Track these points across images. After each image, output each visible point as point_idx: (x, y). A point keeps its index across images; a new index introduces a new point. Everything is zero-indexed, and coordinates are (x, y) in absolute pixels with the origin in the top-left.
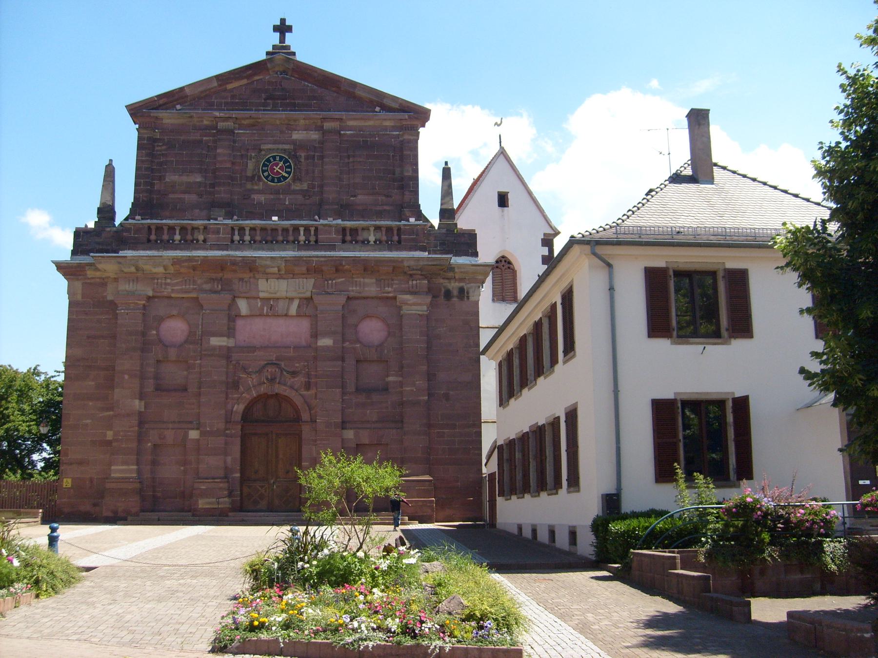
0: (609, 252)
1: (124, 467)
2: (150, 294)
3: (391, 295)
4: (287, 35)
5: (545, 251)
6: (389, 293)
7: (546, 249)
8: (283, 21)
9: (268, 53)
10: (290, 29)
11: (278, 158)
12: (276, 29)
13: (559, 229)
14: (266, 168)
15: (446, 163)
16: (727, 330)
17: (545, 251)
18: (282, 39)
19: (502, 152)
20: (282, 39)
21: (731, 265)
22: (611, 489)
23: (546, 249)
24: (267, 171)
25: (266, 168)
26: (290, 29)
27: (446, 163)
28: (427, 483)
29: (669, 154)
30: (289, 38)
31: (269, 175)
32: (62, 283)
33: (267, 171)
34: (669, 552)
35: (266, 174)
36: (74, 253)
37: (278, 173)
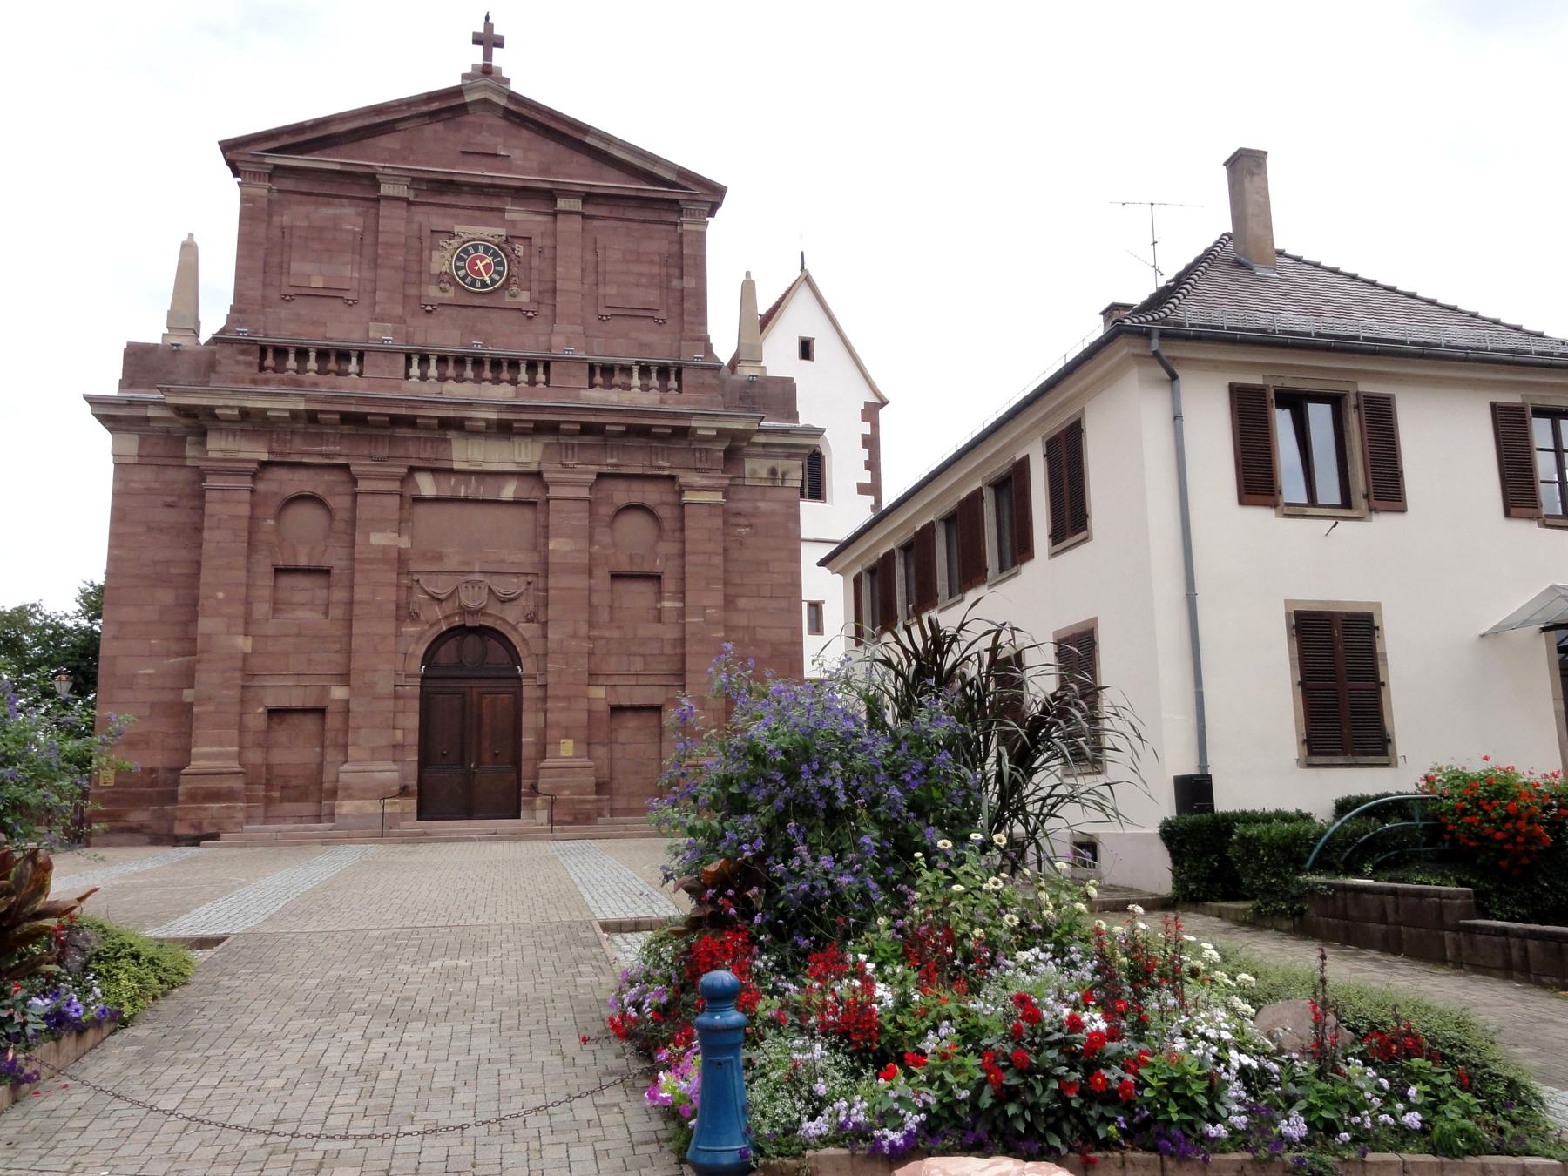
0: (1176, 353)
1: (214, 749)
2: (265, 457)
3: (666, 473)
4: (496, 50)
5: (866, 428)
6: (662, 468)
7: (868, 425)
8: (488, 25)
9: (464, 76)
10: (499, 43)
11: (481, 249)
12: (477, 40)
13: (887, 396)
14: (462, 264)
15: (748, 274)
16: (1366, 497)
17: (866, 428)
18: (487, 55)
19: (806, 279)
20: (487, 55)
21: (1367, 387)
22: (1190, 768)
23: (868, 425)
24: (465, 260)
25: (462, 264)
26: (499, 43)
27: (748, 274)
28: (181, 829)
29: (1154, 243)
30: (499, 58)
31: (467, 275)
32: (101, 440)
33: (464, 268)
34: (1390, 880)
35: (462, 273)
36: (125, 383)
37: (479, 273)
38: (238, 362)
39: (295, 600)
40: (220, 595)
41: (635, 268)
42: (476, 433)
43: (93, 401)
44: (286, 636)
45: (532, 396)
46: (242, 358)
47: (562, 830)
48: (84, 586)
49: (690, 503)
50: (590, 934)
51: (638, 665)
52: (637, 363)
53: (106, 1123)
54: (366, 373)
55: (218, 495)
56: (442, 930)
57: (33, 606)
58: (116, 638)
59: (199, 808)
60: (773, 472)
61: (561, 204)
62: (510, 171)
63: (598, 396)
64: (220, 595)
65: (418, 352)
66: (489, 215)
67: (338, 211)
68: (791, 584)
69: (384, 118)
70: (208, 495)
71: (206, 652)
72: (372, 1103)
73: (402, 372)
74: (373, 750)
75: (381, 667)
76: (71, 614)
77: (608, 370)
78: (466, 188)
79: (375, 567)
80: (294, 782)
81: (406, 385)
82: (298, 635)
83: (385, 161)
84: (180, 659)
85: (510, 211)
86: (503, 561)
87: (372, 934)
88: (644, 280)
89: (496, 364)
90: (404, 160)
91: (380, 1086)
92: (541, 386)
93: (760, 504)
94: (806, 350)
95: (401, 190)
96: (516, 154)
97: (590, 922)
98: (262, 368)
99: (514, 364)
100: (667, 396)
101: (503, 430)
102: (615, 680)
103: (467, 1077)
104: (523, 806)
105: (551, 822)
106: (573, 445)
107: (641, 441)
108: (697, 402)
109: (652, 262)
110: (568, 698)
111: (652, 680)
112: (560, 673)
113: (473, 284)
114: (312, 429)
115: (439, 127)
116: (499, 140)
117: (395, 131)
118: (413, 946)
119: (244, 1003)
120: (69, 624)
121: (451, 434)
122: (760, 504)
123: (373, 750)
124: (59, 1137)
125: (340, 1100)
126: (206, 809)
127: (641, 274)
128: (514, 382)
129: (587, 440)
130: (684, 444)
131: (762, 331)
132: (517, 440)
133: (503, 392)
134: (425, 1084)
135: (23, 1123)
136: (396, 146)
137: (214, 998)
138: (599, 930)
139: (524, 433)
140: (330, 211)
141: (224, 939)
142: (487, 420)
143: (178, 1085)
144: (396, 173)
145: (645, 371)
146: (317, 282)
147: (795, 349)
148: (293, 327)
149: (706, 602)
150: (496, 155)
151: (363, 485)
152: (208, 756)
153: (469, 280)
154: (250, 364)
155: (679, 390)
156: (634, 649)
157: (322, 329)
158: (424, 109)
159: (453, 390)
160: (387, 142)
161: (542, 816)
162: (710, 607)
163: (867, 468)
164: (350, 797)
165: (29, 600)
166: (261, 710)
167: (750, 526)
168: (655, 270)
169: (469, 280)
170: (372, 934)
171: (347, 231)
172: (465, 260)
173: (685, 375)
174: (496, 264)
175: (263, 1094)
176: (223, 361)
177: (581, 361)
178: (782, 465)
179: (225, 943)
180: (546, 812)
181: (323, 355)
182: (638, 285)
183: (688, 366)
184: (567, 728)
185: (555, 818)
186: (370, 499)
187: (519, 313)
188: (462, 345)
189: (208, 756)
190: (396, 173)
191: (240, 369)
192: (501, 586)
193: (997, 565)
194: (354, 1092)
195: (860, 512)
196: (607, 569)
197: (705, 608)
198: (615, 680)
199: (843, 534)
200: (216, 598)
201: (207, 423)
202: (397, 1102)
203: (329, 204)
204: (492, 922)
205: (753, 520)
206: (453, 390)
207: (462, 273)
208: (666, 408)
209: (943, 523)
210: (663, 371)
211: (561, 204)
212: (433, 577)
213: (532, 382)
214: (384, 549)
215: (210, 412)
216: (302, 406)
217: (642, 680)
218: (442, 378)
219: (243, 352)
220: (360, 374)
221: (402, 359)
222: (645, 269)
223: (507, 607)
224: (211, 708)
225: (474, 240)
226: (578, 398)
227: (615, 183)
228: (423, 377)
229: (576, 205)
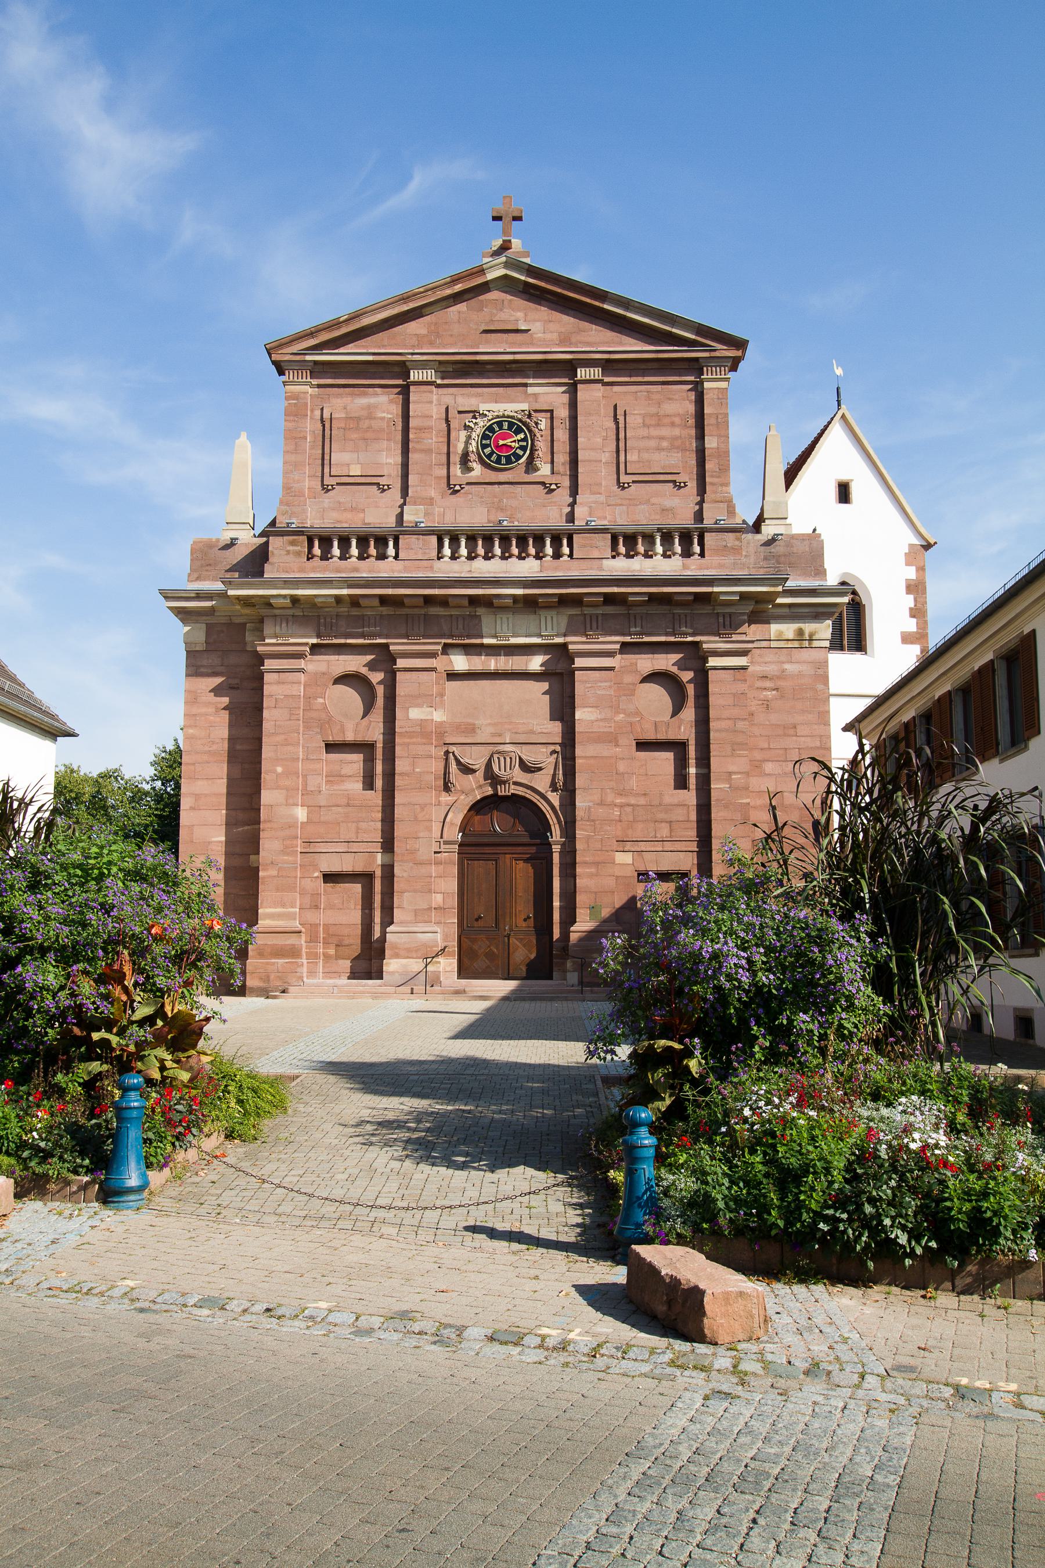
14: (488, 442)
17: (911, 573)
25: (488, 442)
31: (493, 452)
35: (488, 451)
38: (288, 552)
39: (343, 772)
40: (279, 769)
41: (654, 432)
42: (504, 608)
43: (167, 595)
44: (338, 806)
45: (556, 569)
46: (291, 548)
47: (592, 992)
48: (157, 751)
49: (715, 668)
50: (591, 1086)
51: (664, 832)
52: (659, 530)
53: (233, 1193)
54: (401, 555)
55: (275, 676)
56: (469, 1078)
57: (116, 770)
58: (192, 808)
59: (267, 964)
60: (800, 632)
61: (582, 373)
62: (532, 344)
63: (622, 566)
64: (279, 769)
65: (448, 532)
66: (510, 391)
67: (372, 400)
68: (820, 748)
69: (412, 305)
70: (267, 677)
71: (270, 821)
72: (406, 1192)
73: (434, 553)
74: (416, 912)
75: (421, 835)
76: (148, 779)
77: (630, 540)
78: (489, 367)
79: (414, 740)
80: (346, 942)
81: (437, 564)
82: (348, 805)
83: (413, 347)
84: (246, 828)
85: (532, 385)
86: (532, 732)
87: (411, 1078)
88: (665, 444)
89: (522, 540)
90: (431, 344)
91: (413, 1182)
92: (565, 558)
93: (787, 666)
94: (844, 493)
95: (429, 375)
96: (536, 328)
97: (594, 1076)
98: (310, 557)
99: (539, 539)
100: (688, 561)
101: (529, 604)
102: (642, 846)
103: (475, 1181)
104: (555, 969)
105: (581, 983)
106: (597, 616)
107: (664, 609)
108: (721, 566)
109: (673, 424)
110: (596, 864)
111: (678, 846)
112: (588, 838)
113: (498, 461)
114: (355, 612)
115: (462, 307)
116: (520, 315)
117: (423, 316)
118: (444, 1089)
119: (315, 1123)
120: (147, 787)
121: (480, 611)
122: (787, 666)
123: (416, 912)
124: (205, 1198)
125: (386, 1189)
126: (274, 963)
127: (662, 438)
128: (538, 557)
129: (610, 610)
130: (707, 609)
131: (787, 488)
132: (543, 613)
133: (529, 568)
134: (445, 1184)
135: (181, 1189)
136: (423, 331)
137: (294, 1119)
138: (599, 1083)
139: (548, 607)
140: (363, 401)
141: (297, 1077)
142: (514, 596)
143: (276, 1173)
144: (425, 358)
145: (667, 537)
146: (356, 470)
147: (833, 492)
148: (335, 515)
149: (732, 768)
150: (517, 331)
151: (401, 663)
152: (272, 916)
153: (494, 457)
154: (298, 554)
155: (702, 554)
156: (661, 816)
157: (362, 515)
158: (448, 292)
159: (482, 568)
160: (414, 327)
161: (573, 978)
162: (735, 773)
163: (912, 616)
164: (397, 956)
165: (112, 766)
166: (316, 874)
167: (777, 689)
168: (677, 432)
169: (494, 457)
170: (411, 1078)
171: (383, 419)
172: (490, 438)
173: (708, 536)
174: (515, 454)
175: (333, 1182)
176: (276, 552)
177: (603, 531)
178: (808, 627)
179: (298, 1080)
180: (576, 974)
181: (363, 541)
182: (659, 449)
183: (711, 530)
184: (596, 893)
185: (585, 980)
186: (408, 675)
187: (541, 487)
188: (489, 522)
189: (272, 916)
190: (425, 358)
191: (291, 558)
192: (530, 755)
193: (1008, 739)
194: (395, 1185)
195: (909, 658)
196: (632, 737)
197: (730, 773)
198: (642, 846)
199: (880, 688)
200: (275, 771)
201: (264, 612)
202: (424, 1193)
203: (365, 394)
204: (511, 1072)
205: (781, 683)
206: (482, 568)
207: (488, 451)
208: (689, 573)
209: (960, 693)
210: (686, 537)
211: (582, 373)
212: (467, 748)
213: (557, 555)
214: (422, 723)
215: (266, 602)
216: (345, 592)
217: (668, 846)
218: (471, 557)
219: (293, 543)
220: (396, 557)
221: (434, 540)
222: (665, 432)
223: (537, 775)
224: (274, 873)
225: (498, 417)
226: (601, 569)
227: (631, 346)
228: (453, 557)
229: (596, 373)
